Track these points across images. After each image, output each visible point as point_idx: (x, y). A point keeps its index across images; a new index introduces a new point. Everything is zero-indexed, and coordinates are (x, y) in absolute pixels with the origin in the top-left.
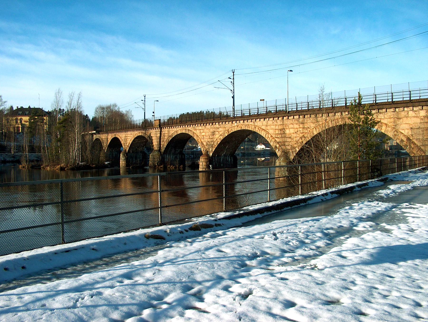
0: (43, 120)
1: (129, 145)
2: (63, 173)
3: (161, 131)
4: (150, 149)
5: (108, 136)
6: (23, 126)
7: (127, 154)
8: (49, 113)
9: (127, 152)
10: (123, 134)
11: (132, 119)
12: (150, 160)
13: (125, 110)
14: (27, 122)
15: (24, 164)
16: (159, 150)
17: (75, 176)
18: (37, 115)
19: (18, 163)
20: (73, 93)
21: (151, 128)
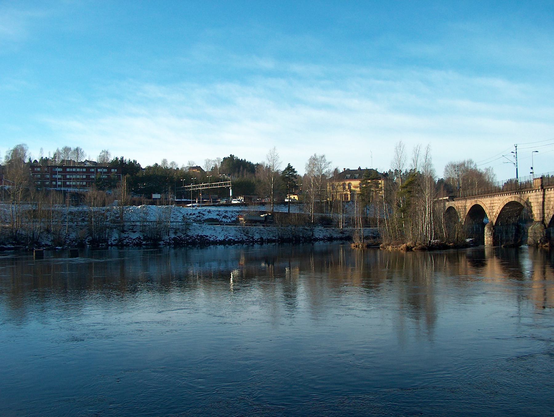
0: (378, 184)
1: (497, 215)
2: (410, 254)
3: (544, 195)
4: (529, 219)
5: (466, 203)
6: (353, 193)
7: (494, 227)
8: (385, 175)
9: (494, 224)
10: (487, 199)
11: (494, 179)
12: (529, 235)
13: (485, 168)
14: (357, 187)
15: (357, 242)
16: (543, 222)
17: (426, 258)
18: (370, 178)
19: (349, 241)
20: (418, 147)
21: (529, 190)
